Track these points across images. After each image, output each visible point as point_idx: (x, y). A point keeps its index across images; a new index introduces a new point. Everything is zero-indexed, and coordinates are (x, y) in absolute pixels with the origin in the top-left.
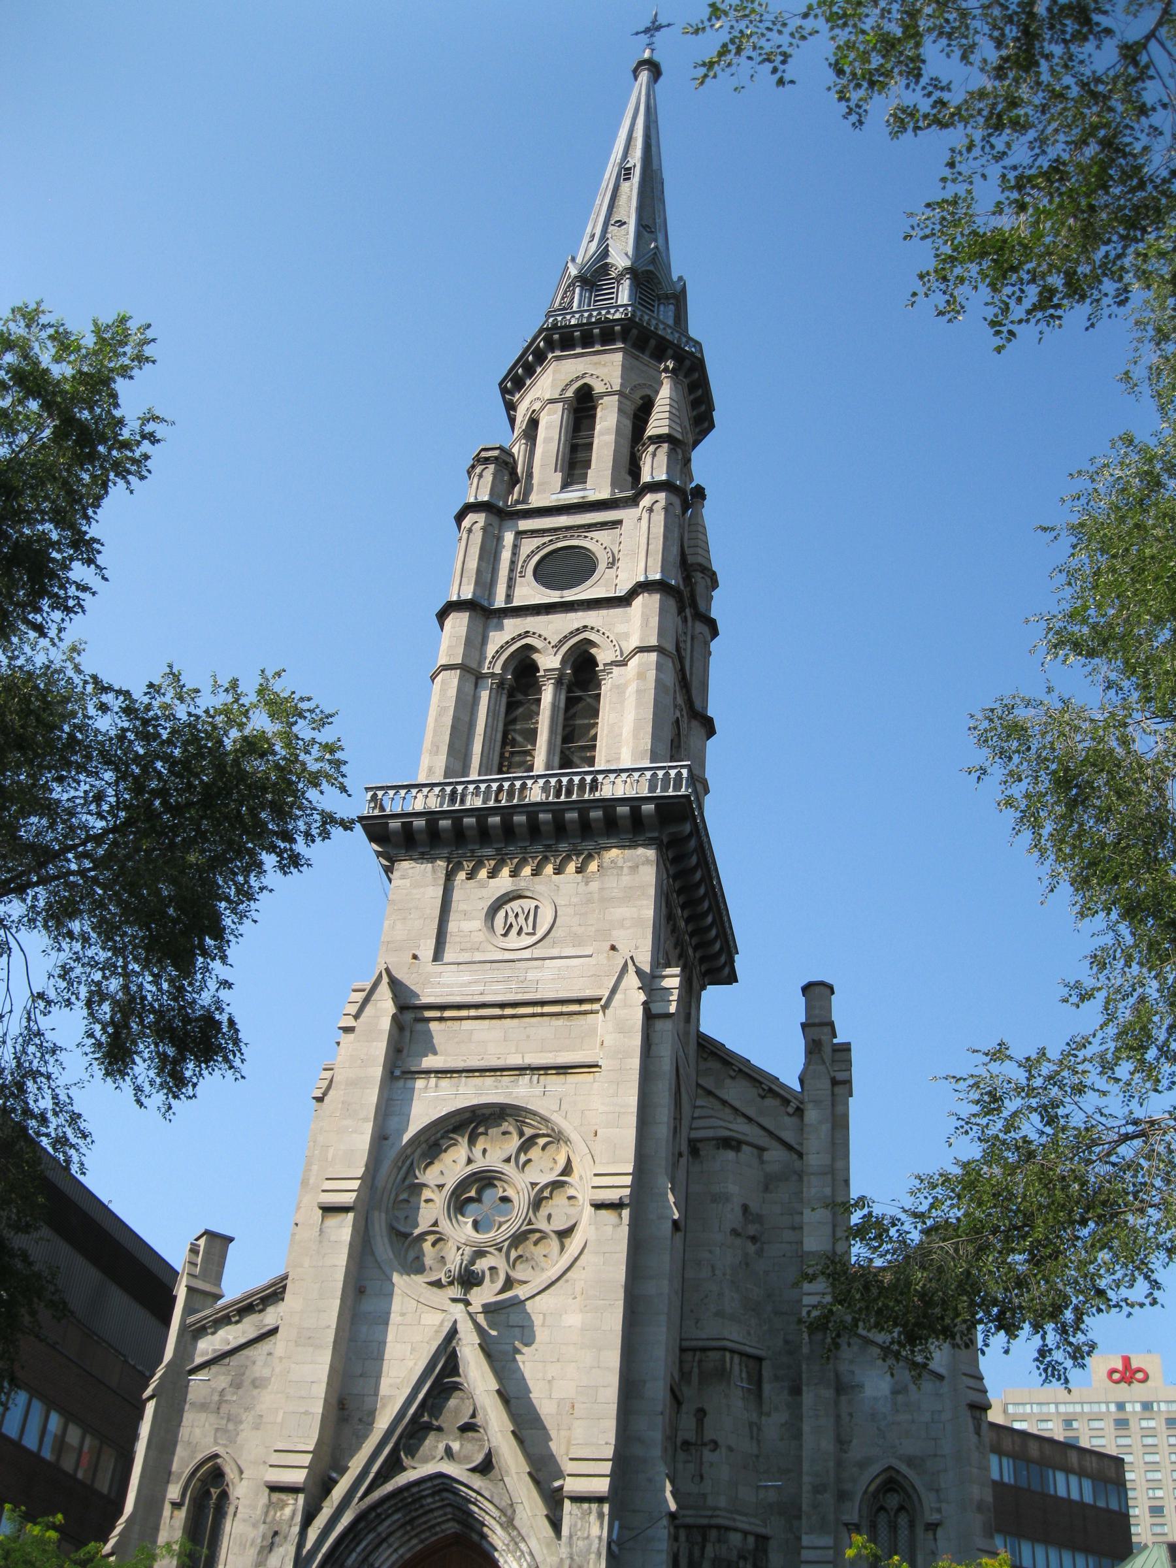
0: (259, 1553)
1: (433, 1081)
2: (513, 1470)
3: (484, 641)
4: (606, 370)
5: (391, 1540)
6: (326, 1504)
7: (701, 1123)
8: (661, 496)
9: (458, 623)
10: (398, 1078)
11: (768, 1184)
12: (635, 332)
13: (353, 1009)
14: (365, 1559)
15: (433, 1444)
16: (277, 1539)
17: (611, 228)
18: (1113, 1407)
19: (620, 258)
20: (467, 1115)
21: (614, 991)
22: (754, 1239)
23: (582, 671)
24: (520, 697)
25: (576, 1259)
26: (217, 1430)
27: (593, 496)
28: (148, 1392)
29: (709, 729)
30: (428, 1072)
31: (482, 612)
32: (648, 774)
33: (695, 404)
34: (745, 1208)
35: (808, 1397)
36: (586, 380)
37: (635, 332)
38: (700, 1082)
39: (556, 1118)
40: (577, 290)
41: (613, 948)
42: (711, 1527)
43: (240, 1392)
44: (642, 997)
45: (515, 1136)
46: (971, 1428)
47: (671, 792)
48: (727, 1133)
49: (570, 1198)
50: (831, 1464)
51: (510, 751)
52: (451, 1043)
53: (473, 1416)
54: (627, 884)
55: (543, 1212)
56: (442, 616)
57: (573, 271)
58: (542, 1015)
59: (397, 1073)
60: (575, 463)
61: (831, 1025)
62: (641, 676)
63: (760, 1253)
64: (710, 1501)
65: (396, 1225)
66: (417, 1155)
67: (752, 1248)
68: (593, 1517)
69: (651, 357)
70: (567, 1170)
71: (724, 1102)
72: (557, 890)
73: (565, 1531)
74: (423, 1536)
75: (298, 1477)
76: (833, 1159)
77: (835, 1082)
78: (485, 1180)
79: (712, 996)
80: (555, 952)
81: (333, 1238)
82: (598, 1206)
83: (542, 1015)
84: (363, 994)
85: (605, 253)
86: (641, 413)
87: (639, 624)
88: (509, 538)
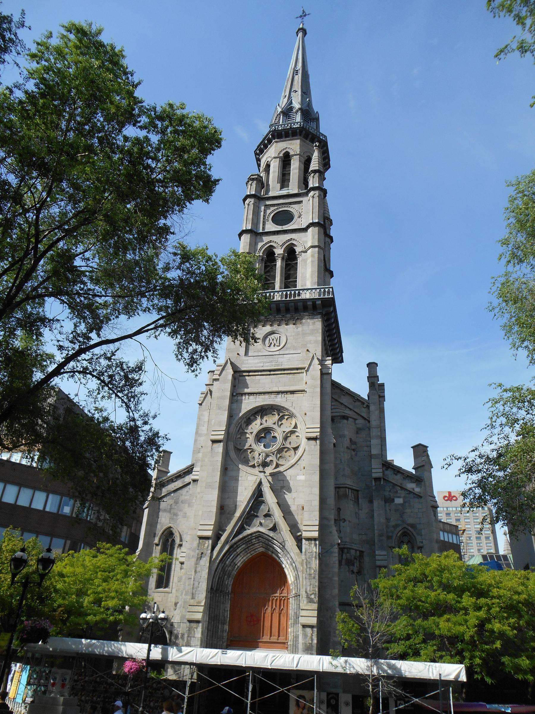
0: (197, 560)
1: (247, 397)
2: (284, 530)
3: (256, 244)
4: (294, 146)
5: (241, 554)
6: (219, 542)
7: (334, 411)
8: (317, 192)
9: (246, 238)
10: (235, 396)
11: (358, 431)
12: (304, 132)
13: (218, 372)
14: (233, 561)
15: (256, 521)
16: (203, 555)
17: (292, 93)
18: (445, 509)
19: (296, 105)
20: (260, 408)
21: (310, 365)
22: (354, 450)
23: (291, 255)
24: (269, 264)
25: (301, 457)
26: (170, 518)
28: (145, 506)
30: (245, 394)
31: (255, 233)
32: (318, 290)
33: (324, 159)
35: (375, 503)
36: (287, 150)
37: (304, 132)
38: (333, 397)
39: (290, 409)
40: (281, 116)
41: (308, 350)
42: (345, 548)
43: (178, 505)
44: (320, 367)
45: (277, 415)
46: (432, 513)
47: (326, 296)
48: (344, 414)
49: (297, 436)
50: (385, 526)
52: (254, 384)
53: (269, 511)
54: (312, 329)
55: (288, 441)
56: (240, 235)
57: (279, 110)
58: (284, 374)
59: (235, 394)
60: (284, 180)
62: (313, 256)
63: (356, 455)
65: (236, 446)
67: (353, 453)
68: (313, 545)
69: (310, 141)
70: (296, 427)
71: (342, 404)
72: (287, 331)
73: (303, 550)
74: (252, 553)
75: (209, 533)
76: (380, 423)
78: (267, 431)
81: (216, 451)
82: (309, 439)
83: (284, 374)
84: (222, 367)
85: (291, 103)
86: (307, 162)
87: (311, 237)
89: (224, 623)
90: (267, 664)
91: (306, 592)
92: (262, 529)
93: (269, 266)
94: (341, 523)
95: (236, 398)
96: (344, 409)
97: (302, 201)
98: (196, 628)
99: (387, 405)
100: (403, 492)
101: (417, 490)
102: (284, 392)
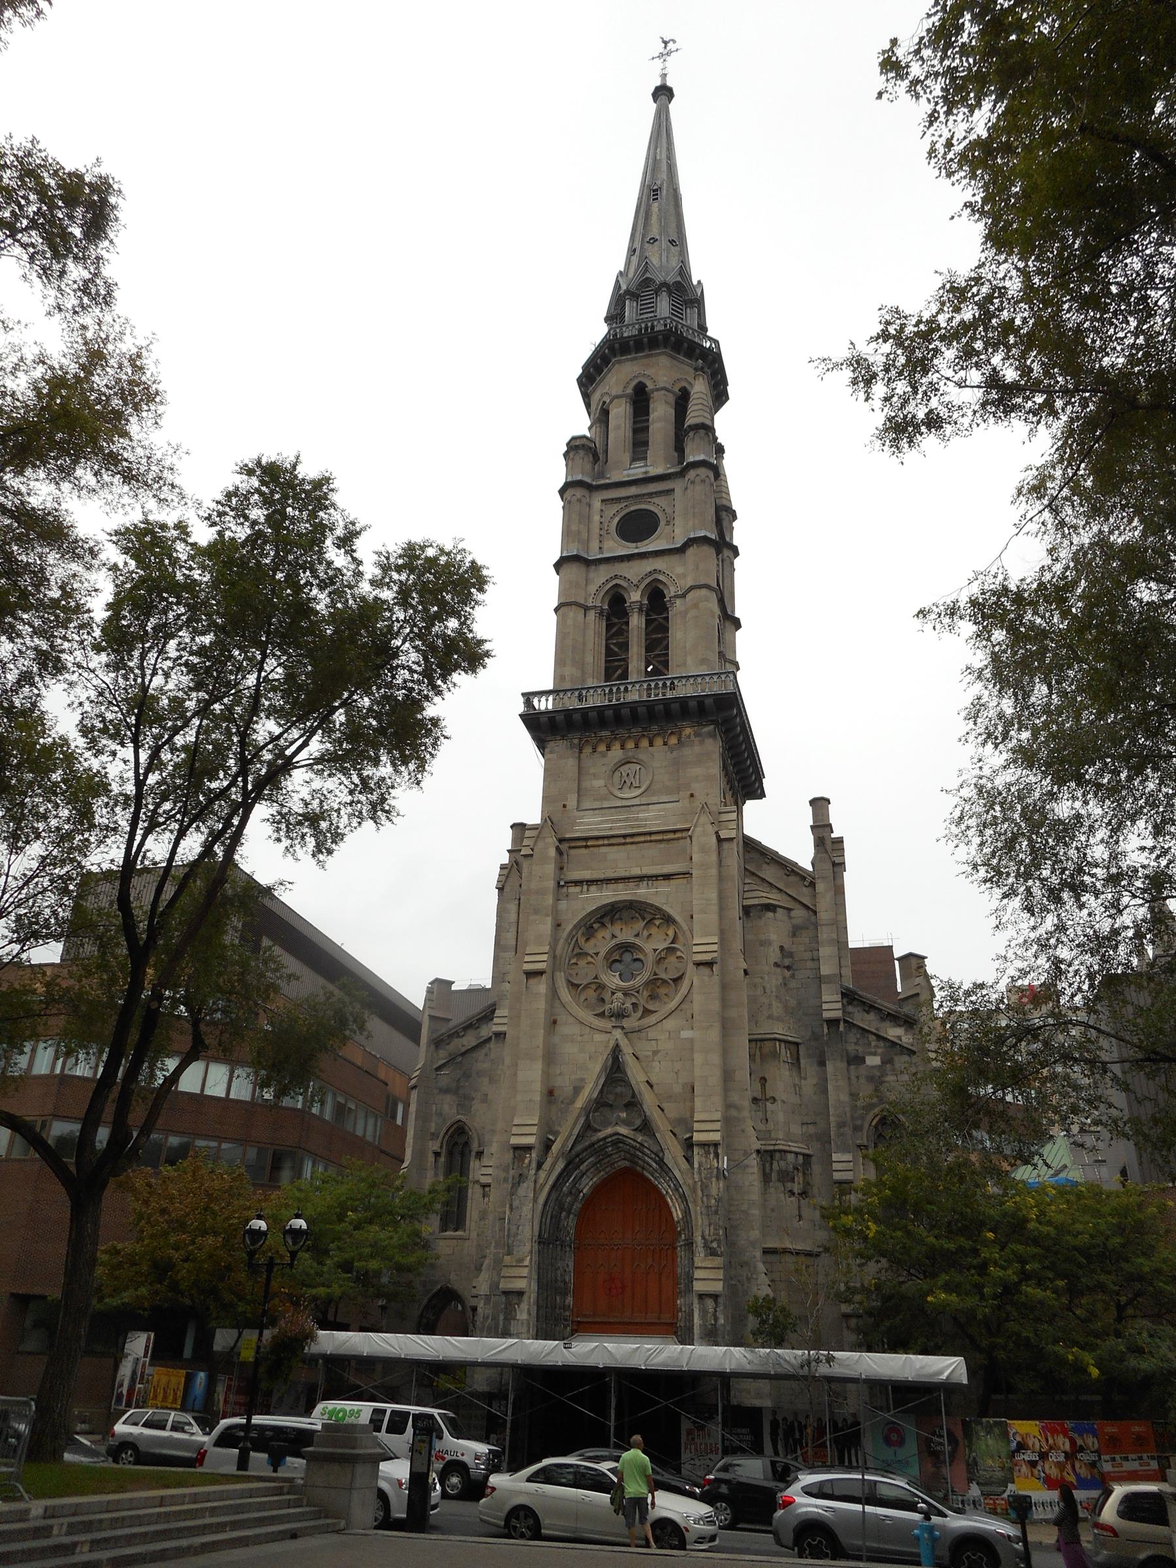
6: (550, 1155)
7: (747, 895)
11: (795, 931)
22: (788, 968)
27: (654, 471)
29: (737, 624)
34: (782, 948)
35: (830, 1067)
41: (692, 795)
42: (775, 1151)
50: (847, 1109)
51: (615, 668)
59: (562, 883)
61: (830, 826)
63: (793, 976)
64: (773, 1135)
66: (579, 934)
67: (788, 974)
71: (763, 880)
72: (657, 756)
73: (696, 1165)
77: (834, 864)
78: (626, 947)
79: (750, 806)
80: (655, 799)
82: (698, 964)
88: (597, 504)
89: (565, 1294)
90: (638, 1362)
91: (703, 1237)
92: (623, 1130)
93: (615, 624)
94: (768, 1104)
95: (565, 889)
96: (768, 889)
97: (673, 490)
98: (518, 1305)
99: (849, 878)
100: (882, 1044)
101: (907, 1039)
102: (652, 877)
